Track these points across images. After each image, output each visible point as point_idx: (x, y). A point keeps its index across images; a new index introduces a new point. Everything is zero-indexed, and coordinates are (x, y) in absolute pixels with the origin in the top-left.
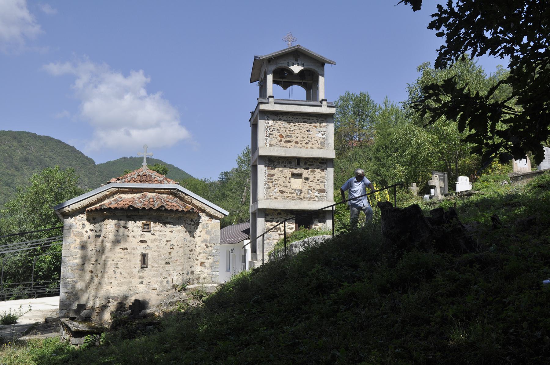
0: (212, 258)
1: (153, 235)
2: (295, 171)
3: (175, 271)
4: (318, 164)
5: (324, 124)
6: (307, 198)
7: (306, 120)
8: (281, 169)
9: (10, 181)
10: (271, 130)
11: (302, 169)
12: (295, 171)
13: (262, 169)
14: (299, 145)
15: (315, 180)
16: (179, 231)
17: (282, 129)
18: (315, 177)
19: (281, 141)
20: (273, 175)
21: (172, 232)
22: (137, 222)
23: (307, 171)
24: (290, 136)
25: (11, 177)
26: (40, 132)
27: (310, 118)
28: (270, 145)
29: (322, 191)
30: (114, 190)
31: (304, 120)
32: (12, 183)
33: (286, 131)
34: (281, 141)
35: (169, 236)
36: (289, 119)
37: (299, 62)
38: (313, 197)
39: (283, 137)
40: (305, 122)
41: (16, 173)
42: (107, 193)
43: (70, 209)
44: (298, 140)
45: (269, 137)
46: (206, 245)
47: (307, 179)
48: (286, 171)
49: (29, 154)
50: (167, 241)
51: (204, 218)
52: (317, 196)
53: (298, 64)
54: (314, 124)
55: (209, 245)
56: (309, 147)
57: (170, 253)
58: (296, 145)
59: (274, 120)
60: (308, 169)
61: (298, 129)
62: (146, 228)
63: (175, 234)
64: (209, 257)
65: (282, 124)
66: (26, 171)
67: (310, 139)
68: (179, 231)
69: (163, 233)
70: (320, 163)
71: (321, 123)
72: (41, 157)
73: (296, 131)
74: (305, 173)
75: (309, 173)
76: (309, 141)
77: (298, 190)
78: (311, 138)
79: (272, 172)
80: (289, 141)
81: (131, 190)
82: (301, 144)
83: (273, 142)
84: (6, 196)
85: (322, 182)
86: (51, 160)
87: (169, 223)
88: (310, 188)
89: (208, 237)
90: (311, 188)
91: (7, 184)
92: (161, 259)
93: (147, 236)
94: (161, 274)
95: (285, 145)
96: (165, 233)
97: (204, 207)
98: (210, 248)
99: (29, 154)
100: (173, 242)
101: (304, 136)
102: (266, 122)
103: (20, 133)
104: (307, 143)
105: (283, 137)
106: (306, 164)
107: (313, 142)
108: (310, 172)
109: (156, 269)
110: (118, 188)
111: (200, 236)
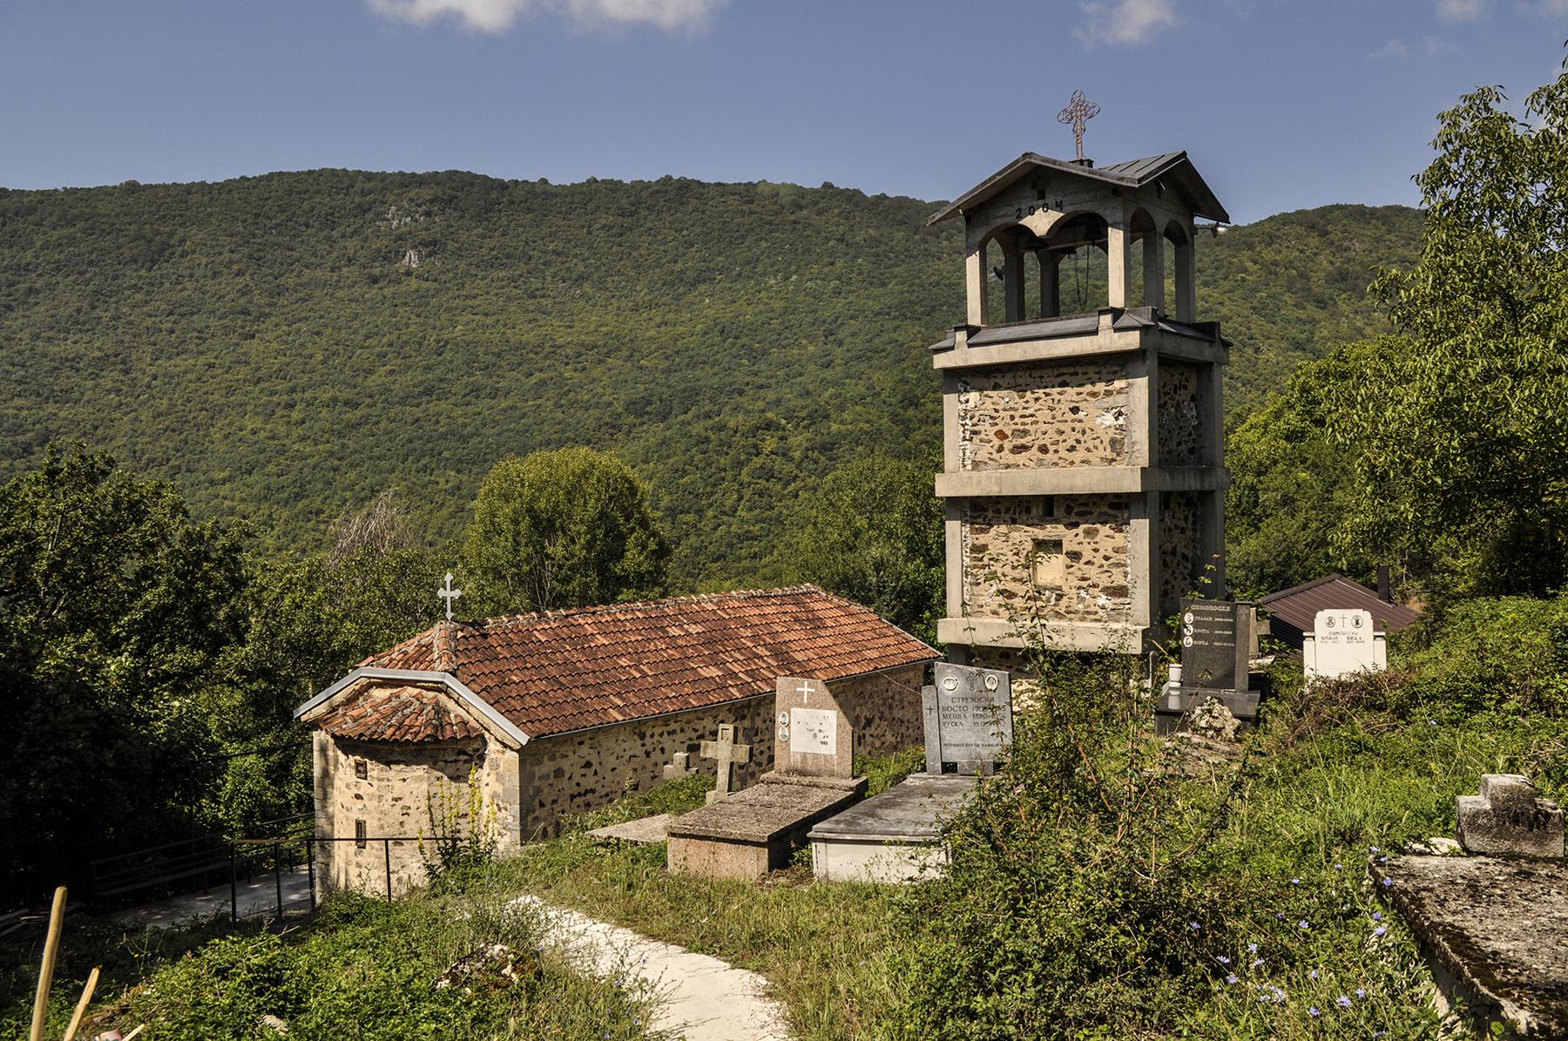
2: (1043, 533)
4: (1105, 509)
5: (1119, 384)
6: (1076, 612)
7: (1067, 378)
8: (1003, 528)
9: (1303, 336)
10: (975, 420)
11: (1061, 527)
12: (1043, 533)
13: (955, 531)
14: (1050, 456)
15: (1099, 560)
16: (420, 779)
17: (1002, 414)
18: (1096, 550)
19: (1000, 449)
20: (984, 548)
23: (1075, 531)
24: (1025, 433)
27: (1079, 370)
28: (976, 465)
29: (1120, 591)
30: (364, 681)
31: (1060, 379)
32: (1310, 340)
33: (1012, 418)
34: (1000, 449)
35: (398, 788)
36: (1020, 381)
37: (1050, 200)
38: (1093, 609)
39: (1006, 437)
40: (1064, 384)
41: (1320, 314)
44: (1047, 442)
45: (971, 440)
47: (1075, 556)
48: (1015, 534)
49: (1348, 261)
50: (396, 800)
51: (493, 746)
52: (1103, 608)
53: (1046, 207)
54: (1088, 388)
56: (1077, 461)
58: (1042, 456)
59: (981, 390)
60: (1076, 525)
61: (1044, 407)
62: (360, 769)
63: (412, 786)
65: (1003, 398)
66: (1343, 307)
67: (1079, 436)
70: (1112, 506)
71: (1110, 381)
73: (1041, 416)
74: (1071, 538)
75: (1081, 538)
76: (1078, 441)
77: (1052, 590)
78: (1084, 432)
79: (982, 539)
80: (1024, 448)
82: (1056, 451)
83: (983, 455)
85: (1118, 565)
87: (398, 763)
88: (1085, 584)
89: (499, 789)
90: (1086, 583)
93: (364, 788)
95: (1012, 459)
99: (1348, 261)
100: (407, 801)
101: (1062, 427)
102: (963, 399)
104: (1072, 449)
105: (1006, 437)
106: (1069, 510)
107: (1090, 444)
108: (1082, 535)
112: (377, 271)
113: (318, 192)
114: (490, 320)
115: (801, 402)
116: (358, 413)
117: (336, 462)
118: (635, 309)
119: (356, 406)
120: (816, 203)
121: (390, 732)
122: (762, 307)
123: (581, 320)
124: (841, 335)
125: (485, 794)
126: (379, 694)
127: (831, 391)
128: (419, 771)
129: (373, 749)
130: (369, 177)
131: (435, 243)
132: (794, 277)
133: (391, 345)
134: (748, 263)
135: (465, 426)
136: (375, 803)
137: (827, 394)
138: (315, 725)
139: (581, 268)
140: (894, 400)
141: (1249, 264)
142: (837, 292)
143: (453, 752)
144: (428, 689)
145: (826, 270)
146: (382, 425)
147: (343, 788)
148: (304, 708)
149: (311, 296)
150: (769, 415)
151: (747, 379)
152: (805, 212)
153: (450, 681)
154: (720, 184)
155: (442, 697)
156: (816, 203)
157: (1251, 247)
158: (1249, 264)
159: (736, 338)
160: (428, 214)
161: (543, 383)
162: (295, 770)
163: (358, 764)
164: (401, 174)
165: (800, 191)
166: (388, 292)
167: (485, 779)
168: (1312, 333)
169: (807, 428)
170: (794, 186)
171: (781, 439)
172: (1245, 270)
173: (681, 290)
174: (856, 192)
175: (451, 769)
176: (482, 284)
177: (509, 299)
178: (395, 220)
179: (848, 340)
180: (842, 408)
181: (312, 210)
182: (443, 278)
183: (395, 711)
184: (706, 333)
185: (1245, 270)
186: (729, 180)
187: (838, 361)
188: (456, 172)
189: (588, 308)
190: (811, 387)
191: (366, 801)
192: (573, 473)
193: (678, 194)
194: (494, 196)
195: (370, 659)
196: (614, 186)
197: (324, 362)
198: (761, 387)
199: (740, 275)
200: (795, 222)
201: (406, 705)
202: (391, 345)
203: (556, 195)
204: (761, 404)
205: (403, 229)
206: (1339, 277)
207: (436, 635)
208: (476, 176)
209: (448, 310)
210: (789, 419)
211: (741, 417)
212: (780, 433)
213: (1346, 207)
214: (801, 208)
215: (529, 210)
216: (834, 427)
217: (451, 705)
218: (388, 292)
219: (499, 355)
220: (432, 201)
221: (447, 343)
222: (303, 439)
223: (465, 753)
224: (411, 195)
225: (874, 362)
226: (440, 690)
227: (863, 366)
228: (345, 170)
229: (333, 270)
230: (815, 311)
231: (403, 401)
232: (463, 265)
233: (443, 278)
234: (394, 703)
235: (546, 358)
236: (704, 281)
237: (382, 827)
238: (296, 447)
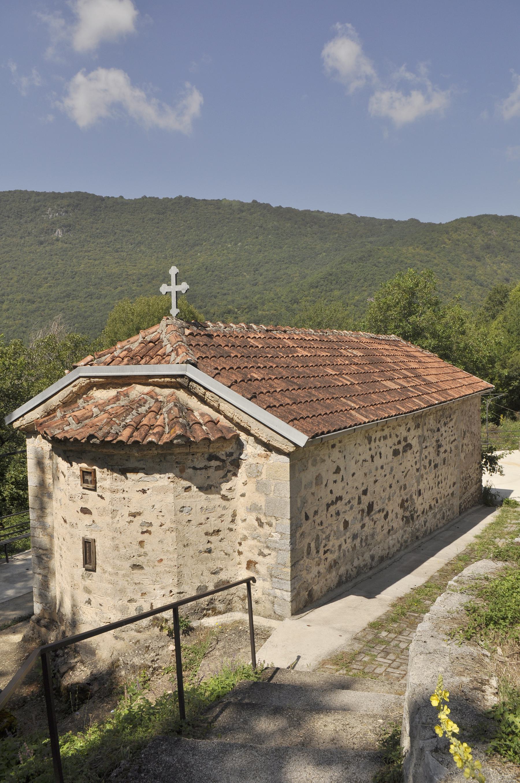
0: (274, 553)
1: (102, 497)
3: (157, 587)
9: (471, 273)
16: (163, 490)
21: (144, 491)
22: (74, 464)
25: (472, 269)
26: (502, 213)
30: (83, 382)
32: (473, 275)
35: (137, 501)
41: (478, 264)
42: (75, 389)
43: (24, 422)
46: (258, 520)
49: (490, 239)
50: (134, 515)
51: (251, 451)
55: (264, 520)
57: (141, 543)
62: (88, 480)
63: (152, 498)
64: (266, 551)
66: (488, 260)
68: (163, 490)
69: (120, 495)
72: (504, 241)
81: (109, 381)
84: (468, 291)
86: (516, 244)
87: (135, 471)
89: (261, 500)
91: (469, 278)
92: (120, 557)
94: (122, 591)
96: (125, 495)
97: (245, 420)
98: (266, 527)
103: (480, 217)
109: (109, 578)
110: (89, 377)
111: (243, 495)
112: (42, 239)
113: (13, 201)
114: (97, 262)
115: (244, 301)
116: (34, 306)
117: (24, 329)
118: (165, 258)
119: (34, 302)
120: (249, 210)
121: (127, 432)
122: (225, 257)
123: (140, 263)
124: (261, 270)
125: (240, 505)
126: (101, 395)
127: (258, 296)
128: (162, 481)
129: (102, 454)
130: (38, 194)
131: (70, 226)
132: (240, 244)
133: (50, 274)
134: (218, 237)
135: (86, 312)
136: (108, 519)
137: (256, 298)
138: (31, 431)
139: (139, 238)
140: (287, 300)
141: (447, 240)
142: (260, 251)
143: (205, 458)
144: (162, 386)
145: (254, 240)
146: (46, 311)
147: (66, 500)
148: (18, 412)
149: (11, 250)
150: (229, 307)
151: (218, 291)
152: (244, 214)
153: (192, 372)
154: (204, 200)
155: (182, 394)
156: (249, 210)
157: (447, 233)
158: (447, 240)
159: (213, 272)
160: (66, 212)
161: (122, 292)
162: (8, 476)
163: (84, 473)
164: (53, 193)
165: (242, 204)
166: (48, 248)
167: (240, 488)
168: (475, 272)
169: (247, 313)
170: (239, 201)
171: (236, 318)
172: (445, 243)
173: (187, 249)
174: (268, 205)
175: (200, 476)
176: (93, 245)
177: (106, 252)
178: (51, 215)
179: (265, 273)
180: (263, 304)
181: (11, 209)
182: (74, 242)
183: (128, 409)
184: (199, 269)
185: (445, 243)
186: (209, 198)
187: (260, 283)
188: (80, 192)
189: (143, 257)
190: (248, 295)
191: (95, 515)
192: (162, 309)
193: (185, 203)
194: (97, 204)
195: (89, 358)
196: (155, 200)
197: (18, 282)
198: (225, 294)
199: (214, 242)
200: (240, 218)
201: (141, 403)
202: (50, 274)
203: (127, 204)
204: (225, 302)
205: (55, 219)
206: (487, 247)
207: (165, 331)
208: (89, 195)
209: (77, 257)
210: (239, 309)
211: (216, 308)
212: (235, 315)
213: (489, 215)
214: (243, 211)
215: (114, 211)
216: (260, 313)
217: (193, 402)
218: (48, 248)
219: (101, 279)
220: (68, 206)
221: (76, 273)
222: (8, 318)
223: (217, 458)
224: (59, 203)
225: (277, 284)
226: (178, 386)
227: (272, 285)
228: (26, 191)
229: (21, 238)
230: (249, 260)
231: (56, 300)
232: (83, 236)
233: (74, 242)
234: (123, 402)
235: (124, 280)
236: (197, 245)
237: (117, 548)
238: (5, 321)
